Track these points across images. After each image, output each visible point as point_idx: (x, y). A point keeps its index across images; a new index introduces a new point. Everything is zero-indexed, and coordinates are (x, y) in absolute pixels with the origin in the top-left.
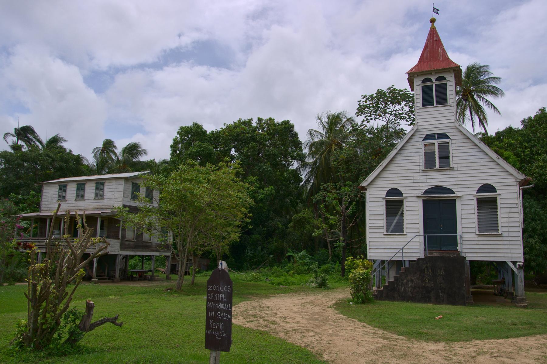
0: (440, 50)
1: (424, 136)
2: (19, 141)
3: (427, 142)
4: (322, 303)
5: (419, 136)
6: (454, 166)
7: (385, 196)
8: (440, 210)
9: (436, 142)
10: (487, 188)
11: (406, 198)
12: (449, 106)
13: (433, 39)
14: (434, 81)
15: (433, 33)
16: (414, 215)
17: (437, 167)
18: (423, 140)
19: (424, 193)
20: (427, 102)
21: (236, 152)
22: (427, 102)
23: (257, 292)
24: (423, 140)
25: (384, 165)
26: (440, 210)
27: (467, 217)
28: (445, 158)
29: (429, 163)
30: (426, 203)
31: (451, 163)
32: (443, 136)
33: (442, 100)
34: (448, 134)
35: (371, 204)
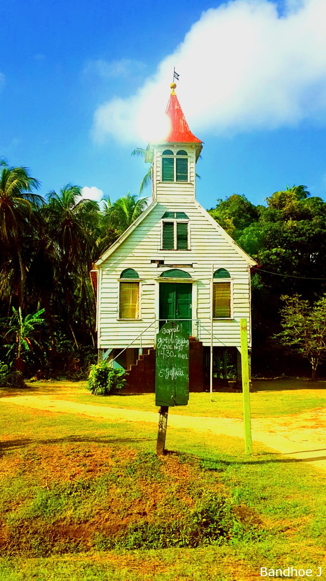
0: (181, 122)
1: (164, 213)
2: (243, 435)
3: (166, 220)
4: (81, 388)
5: (157, 213)
6: (192, 248)
7: (119, 277)
8: (175, 296)
9: (175, 221)
10: (221, 273)
11: (142, 280)
12: (189, 184)
13: (174, 106)
14: (175, 154)
15: (174, 100)
16: (149, 300)
17: (175, 248)
18: (162, 218)
19: (161, 275)
20: (166, 177)
21: (31, 334)
22: (166, 177)
23: (15, 393)
24: (162, 218)
25: (121, 242)
26: (175, 296)
27: (201, 301)
28: (183, 239)
29: (167, 245)
30: (162, 286)
31: (189, 245)
32: (182, 215)
33: (182, 176)
34: (187, 214)
35: (104, 285)
